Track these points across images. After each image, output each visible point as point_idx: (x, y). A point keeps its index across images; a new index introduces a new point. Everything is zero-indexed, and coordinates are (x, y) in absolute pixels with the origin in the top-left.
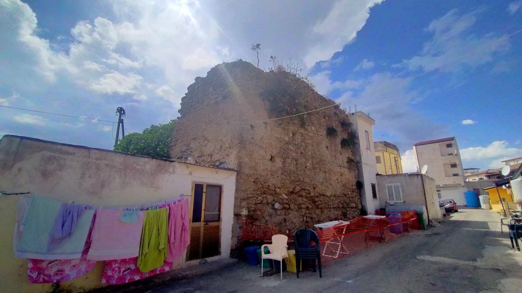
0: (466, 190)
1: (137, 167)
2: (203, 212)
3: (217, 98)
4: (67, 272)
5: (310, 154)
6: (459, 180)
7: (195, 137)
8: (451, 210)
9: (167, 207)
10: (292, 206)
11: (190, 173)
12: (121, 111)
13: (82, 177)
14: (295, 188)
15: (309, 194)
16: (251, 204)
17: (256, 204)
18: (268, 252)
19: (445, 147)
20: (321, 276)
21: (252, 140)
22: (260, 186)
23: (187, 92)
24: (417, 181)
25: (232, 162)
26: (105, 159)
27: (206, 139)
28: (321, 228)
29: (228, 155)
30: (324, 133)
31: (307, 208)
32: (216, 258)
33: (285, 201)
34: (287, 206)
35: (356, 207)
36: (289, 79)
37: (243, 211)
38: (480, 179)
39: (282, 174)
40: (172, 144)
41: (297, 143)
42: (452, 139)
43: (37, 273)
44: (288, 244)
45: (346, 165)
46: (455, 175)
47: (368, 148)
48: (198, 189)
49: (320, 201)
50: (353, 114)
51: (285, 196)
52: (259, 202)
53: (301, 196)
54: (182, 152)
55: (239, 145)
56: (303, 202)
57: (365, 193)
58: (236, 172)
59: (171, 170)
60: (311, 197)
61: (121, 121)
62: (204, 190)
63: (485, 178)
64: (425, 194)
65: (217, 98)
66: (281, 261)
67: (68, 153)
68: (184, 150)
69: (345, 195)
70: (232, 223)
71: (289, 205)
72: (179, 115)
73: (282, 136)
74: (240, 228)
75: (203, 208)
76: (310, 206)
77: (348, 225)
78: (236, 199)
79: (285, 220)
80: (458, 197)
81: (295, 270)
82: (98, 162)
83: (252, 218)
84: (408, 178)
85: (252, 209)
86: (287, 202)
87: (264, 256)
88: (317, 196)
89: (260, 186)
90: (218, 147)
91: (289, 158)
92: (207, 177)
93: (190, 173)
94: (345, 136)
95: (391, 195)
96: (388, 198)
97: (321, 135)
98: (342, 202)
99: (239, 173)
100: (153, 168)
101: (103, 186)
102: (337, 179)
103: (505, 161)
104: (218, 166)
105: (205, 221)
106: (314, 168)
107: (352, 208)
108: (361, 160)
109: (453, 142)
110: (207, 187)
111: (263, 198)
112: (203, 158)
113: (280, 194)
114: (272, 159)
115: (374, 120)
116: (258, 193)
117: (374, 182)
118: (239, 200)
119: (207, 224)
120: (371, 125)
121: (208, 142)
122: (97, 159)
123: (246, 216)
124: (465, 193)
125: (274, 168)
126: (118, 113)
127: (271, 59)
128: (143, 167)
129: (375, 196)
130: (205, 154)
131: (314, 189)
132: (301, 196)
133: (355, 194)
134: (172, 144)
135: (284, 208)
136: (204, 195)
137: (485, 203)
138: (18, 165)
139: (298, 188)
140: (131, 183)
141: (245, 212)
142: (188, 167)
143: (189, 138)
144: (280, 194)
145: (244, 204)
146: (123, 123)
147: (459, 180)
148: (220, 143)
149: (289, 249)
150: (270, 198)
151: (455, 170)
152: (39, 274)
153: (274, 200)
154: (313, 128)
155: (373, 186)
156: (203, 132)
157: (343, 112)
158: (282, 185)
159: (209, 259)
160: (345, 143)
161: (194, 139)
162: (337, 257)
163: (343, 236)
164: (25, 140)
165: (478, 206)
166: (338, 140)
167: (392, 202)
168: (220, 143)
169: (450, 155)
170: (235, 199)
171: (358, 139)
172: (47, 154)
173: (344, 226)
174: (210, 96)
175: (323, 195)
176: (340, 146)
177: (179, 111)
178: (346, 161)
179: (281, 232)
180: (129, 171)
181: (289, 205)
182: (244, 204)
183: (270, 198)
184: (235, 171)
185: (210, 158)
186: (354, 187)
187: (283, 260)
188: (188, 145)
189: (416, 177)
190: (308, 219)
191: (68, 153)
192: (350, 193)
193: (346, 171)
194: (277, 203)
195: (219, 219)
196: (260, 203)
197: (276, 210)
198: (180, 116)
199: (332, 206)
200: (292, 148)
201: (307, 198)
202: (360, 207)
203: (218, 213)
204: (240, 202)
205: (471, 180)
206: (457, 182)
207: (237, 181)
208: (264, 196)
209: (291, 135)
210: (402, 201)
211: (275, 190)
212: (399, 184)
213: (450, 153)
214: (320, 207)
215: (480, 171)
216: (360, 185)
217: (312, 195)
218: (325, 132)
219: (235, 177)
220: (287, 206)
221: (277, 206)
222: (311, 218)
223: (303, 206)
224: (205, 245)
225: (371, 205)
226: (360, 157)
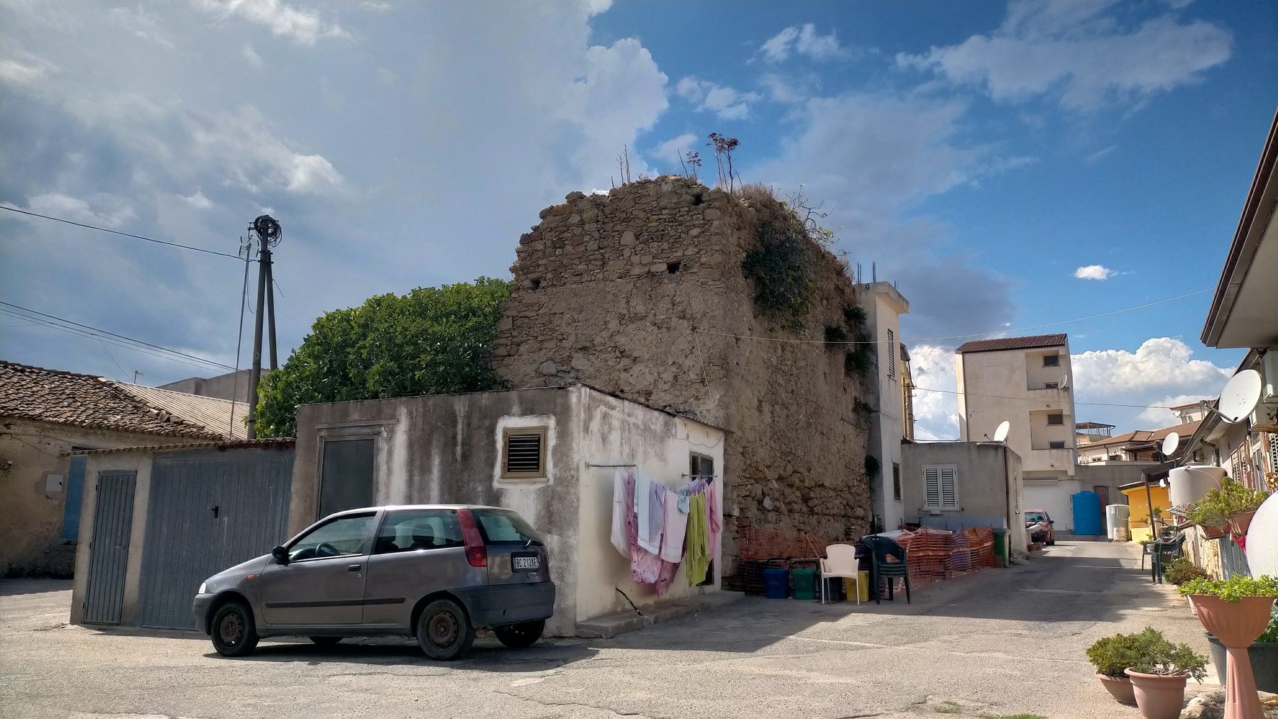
0: (1075, 488)
6: (1061, 461)
8: (1042, 539)
12: (266, 228)
19: (1041, 362)
24: (994, 459)
25: (710, 406)
29: (697, 398)
38: (1112, 458)
42: (1061, 340)
45: (851, 415)
46: (1058, 446)
53: (791, 486)
57: (881, 483)
58: (721, 435)
63: (1124, 457)
64: (1007, 493)
80: (1054, 504)
84: (974, 452)
90: (668, 376)
95: (932, 495)
96: (926, 498)
99: (727, 433)
103: (1181, 409)
106: (809, 425)
107: (857, 518)
108: (878, 404)
109: (1061, 351)
117: (898, 460)
124: (1074, 497)
131: (809, 470)
134: (502, 351)
137: (1116, 524)
143: (566, 344)
147: (1061, 461)
151: (1057, 433)
155: (896, 471)
161: (584, 349)
165: (1099, 533)
167: (935, 510)
168: (674, 369)
169: (1049, 386)
174: (627, 253)
179: (847, 538)
184: (717, 428)
189: (992, 453)
193: (850, 430)
205: (1086, 459)
206: (1059, 467)
207: (725, 450)
210: (957, 507)
212: (954, 467)
213: (1052, 381)
215: (1116, 434)
216: (873, 466)
221: (767, 503)
225: (891, 512)
226: (878, 399)
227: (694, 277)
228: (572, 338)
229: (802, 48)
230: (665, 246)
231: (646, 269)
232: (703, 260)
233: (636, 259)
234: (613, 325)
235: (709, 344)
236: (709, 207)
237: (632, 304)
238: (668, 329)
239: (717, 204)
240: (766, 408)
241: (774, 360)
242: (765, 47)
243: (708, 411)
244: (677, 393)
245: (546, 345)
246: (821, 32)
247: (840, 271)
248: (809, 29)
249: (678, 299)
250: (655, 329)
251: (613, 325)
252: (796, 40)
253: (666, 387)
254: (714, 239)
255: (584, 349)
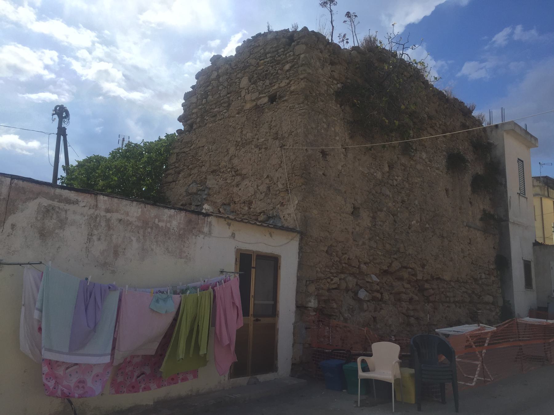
1: (161, 224)
2: (252, 300)
3: (258, 99)
4: (89, 384)
5: (416, 202)
7: (215, 168)
9: (211, 289)
10: (386, 296)
11: (233, 236)
13: (89, 240)
14: (391, 264)
15: (413, 275)
16: (322, 289)
17: (329, 290)
18: (366, 369)
20: (457, 411)
21: (323, 177)
22: (337, 259)
23: (195, 83)
25: (290, 213)
26: (117, 211)
27: (237, 173)
28: (447, 336)
29: (282, 204)
30: (441, 162)
31: (411, 299)
32: (270, 376)
33: (376, 287)
34: (379, 295)
35: (493, 304)
36: (389, 64)
37: (310, 302)
39: (370, 239)
40: (170, 179)
41: (395, 183)
43: (54, 381)
44: (400, 357)
47: (522, 193)
48: (245, 259)
49: (433, 289)
50: (497, 126)
51: (375, 278)
52: (334, 286)
53: (401, 279)
54: (190, 194)
55: (303, 187)
56: (404, 290)
58: (299, 235)
59: (206, 230)
60: (417, 281)
61: (62, 132)
62: (254, 264)
65: (258, 99)
66: (393, 382)
67: (68, 201)
68: (195, 190)
69: (476, 280)
70: (293, 320)
71: (382, 294)
72: (181, 126)
73: (372, 171)
74: (306, 328)
75: (252, 293)
76: (416, 298)
77: (494, 333)
78: (299, 279)
79: (375, 318)
81: (412, 399)
82: (109, 215)
83: (324, 314)
85: (323, 298)
86: (378, 288)
87: (361, 374)
88: (427, 281)
89: (337, 259)
90: (263, 188)
91: (381, 210)
92: (257, 241)
93: (233, 236)
94: (479, 170)
97: (438, 169)
98: (470, 292)
99: (303, 235)
100: (182, 226)
101: (116, 254)
102: (463, 251)
104: (269, 222)
105: (254, 315)
108: (507, 215)
110: (256, 259)
111: (340, 279)
112: (232, 206)
113: (367, 275)
114: (355, 211)
115: (536, 139)
116: (332, 271)
117: (529, 257)
118: (304, 282)
119: (257, 320)
120: (529, 147)
121: (243, 179)
122: (108, 211)
123: (315, 310)
125: (357, 229)
126: (56, 116)
127: (347, 19)
128: (168, 225)
129: (528, 284)
130: (237, 200)
131: (423, 266)
132: (401, 279)
133: (493, 278)
134: (170, 179)
135: (374, 299)
136: (253, 271)
138: (11, 220)
139: (396, 265)
140: (152, 250)
141: (313, 303)
142: (229, 225)
143: (204, 169)
144: (367, 275)
145: (312, 288)
146: (65, 136)
148: (267, 181)
149: (402, 365)
150: (351, 281)
152: (57, 383)
153: (357, 284)
154: (424, 156)
155: (527, 265)
156: (231, 159)
157: (478, 122)
158: (371, 258)
159: (262, 378)
160: (478, 184)
161: (213, 172)
162: (473, 384)
163: (484, 351)
164: (16, 181)
166: (468, 178)
168: (267, 181)
170: (298, 280)
171: (504, 176)
172: (45, 202)
173: (487, 333)
174: (243, 94)
175: (438, 278)
176: (469, 189)
177: (180, 119)
178: (479, 217)
180: (149, 230)
181: (382, 294)
182: (312, 288)
183: (351, 281)
184: (298, 232)
185: (246, 208)
186: (492, 267)
187: (396, 380)
188: (203, 182)
190: (412, 320)
191: (68, 201)
192: (483, 276)
194: (362, 290)
195: (273, 312)
196: (335, 289)
197: (360, 301)
198: (182, 128)
199: (452, 300)
200: (388, 193)
201: (409, 282)
202: (501, 303)
203: (272, 303)
204: (307, 286)
207: (301, 249)
208: (343, 276)
209: (387, 169)
211: (359, 267)
214: (431, 299)
216: (503, 262)
217: (420, 277)
218: (444, 162)
219: (298, 243)
220: (379, 295)
221: (362, 294)
222: (417, 319)
223: (404, 296)
224: (254, 354)
225: (522, 299)
226: (507, 211)
227: (286, 104)
228: (207, 165)
229: (516, 37)
230: (267, 82)
231: (255, 103)
232: (292, 88)
233: (248, 97)
234: (232, 150)
235: (293, 158)
236: (298, 44)
237: (244, 132)
238: (266, 148)
239: (303, 40)
240: (365, 215)
241: (379, 175)
242: (494, 39)
243: (289, 214)
244: (269, 201)
245: (193, 172)
246: (526, 28)
247: (467, 112)
248: (519, 28)
249: (273, 124)
250: (257, 150)
251: (232, 150)
252: (512, 33)
253: (262, 197)
254: (301, 69)
255: (213, 172)
